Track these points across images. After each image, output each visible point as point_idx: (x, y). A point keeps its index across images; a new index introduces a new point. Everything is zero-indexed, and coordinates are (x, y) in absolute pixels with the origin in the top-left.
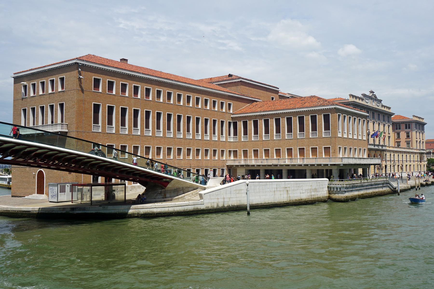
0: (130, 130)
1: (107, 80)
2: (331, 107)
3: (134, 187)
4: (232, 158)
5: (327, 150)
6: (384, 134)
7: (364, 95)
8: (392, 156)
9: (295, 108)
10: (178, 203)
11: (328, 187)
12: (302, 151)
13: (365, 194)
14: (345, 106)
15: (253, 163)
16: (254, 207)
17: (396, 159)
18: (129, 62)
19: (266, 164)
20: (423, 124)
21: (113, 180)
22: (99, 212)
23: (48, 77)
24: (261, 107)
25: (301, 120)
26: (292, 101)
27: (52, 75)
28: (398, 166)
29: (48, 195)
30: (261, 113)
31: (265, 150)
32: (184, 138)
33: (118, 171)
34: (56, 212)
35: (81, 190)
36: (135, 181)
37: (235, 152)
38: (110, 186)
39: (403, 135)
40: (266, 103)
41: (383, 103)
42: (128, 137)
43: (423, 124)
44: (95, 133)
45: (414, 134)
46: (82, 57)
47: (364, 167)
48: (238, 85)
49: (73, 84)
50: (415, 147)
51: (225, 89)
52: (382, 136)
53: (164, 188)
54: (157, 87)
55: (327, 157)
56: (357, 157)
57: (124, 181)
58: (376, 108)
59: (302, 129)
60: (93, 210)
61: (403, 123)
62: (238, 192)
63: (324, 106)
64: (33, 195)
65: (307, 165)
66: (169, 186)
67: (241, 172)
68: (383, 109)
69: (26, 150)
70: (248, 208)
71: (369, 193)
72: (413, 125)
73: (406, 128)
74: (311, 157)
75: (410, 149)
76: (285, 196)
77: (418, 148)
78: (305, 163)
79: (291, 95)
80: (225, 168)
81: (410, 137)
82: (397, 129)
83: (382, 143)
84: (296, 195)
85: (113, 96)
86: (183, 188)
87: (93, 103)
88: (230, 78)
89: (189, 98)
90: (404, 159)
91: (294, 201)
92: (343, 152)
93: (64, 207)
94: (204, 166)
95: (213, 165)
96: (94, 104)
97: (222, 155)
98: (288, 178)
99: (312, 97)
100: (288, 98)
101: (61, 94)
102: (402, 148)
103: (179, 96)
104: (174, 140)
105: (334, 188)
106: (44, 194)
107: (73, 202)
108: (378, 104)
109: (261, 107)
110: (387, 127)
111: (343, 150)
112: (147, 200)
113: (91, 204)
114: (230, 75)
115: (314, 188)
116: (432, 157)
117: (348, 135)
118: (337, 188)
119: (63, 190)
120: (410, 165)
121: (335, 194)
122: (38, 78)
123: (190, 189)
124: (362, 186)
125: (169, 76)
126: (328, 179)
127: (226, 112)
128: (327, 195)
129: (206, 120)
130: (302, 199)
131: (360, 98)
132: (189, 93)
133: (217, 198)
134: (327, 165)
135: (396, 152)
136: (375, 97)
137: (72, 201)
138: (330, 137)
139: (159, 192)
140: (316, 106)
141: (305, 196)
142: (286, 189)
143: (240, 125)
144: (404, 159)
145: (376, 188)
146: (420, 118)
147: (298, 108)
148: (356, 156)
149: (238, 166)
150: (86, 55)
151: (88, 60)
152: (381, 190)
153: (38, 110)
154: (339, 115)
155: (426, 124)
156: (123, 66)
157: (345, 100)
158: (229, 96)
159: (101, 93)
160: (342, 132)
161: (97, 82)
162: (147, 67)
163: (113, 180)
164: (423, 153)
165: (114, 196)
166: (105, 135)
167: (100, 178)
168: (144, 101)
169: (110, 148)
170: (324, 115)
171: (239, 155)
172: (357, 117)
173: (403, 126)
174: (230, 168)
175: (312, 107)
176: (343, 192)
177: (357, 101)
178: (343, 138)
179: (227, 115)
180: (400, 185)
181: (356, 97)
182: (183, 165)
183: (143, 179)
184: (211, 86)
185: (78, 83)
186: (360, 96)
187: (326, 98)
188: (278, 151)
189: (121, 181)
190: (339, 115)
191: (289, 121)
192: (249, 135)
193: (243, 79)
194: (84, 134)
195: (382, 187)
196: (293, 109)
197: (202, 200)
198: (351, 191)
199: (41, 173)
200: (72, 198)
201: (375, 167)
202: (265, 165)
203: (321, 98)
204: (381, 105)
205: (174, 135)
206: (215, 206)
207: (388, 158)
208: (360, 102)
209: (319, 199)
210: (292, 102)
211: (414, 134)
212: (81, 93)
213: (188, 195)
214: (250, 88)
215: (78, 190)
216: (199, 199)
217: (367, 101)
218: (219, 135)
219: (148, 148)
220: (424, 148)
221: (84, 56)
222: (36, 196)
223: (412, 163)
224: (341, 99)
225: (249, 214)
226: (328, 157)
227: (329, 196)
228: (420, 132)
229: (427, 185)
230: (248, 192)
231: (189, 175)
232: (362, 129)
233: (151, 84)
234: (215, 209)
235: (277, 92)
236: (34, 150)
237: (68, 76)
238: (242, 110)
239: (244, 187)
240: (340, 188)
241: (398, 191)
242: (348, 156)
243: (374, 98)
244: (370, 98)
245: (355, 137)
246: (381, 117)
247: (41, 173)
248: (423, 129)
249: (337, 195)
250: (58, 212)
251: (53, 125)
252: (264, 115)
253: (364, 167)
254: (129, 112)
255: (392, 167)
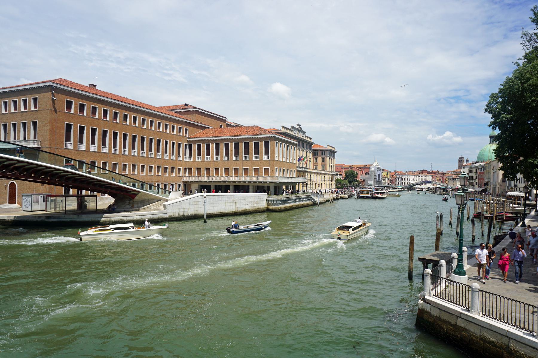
0: (110, 150)
1: (79, 102)
2: (271, 136)
3: (103, 198)
4: (187, 175)
5: (266, 170)
6: (307, 159)
7: (293, 127)
8: (312, 177)
9: (242, 136)
10: (145, 213)
11: (267, 200)
12: (246, 170)
13: (294, 206)
14: (279, 135)
15: (205, 179)
16: (211, 216)
17: (315, 179)
18: (97, 88)
19: (216, 180)
20: (334, 152)
21: (84, 192)
22: (73, 220)
23: (21, 97)
24: (212, 133)
25: (246, 145)
26: (238, 129)
27: (25, 95)
28: (316, 184)
29: (21, 205)
30: (213, 138)
31: (216, 169)
32: (147, 157)
33: (92, 184)
34: (32, 220)
35: (55, 200)
36: (104, 193)
37: (190, 170)
38: (82, 198)
39: (320, 160)
40: (217, 130)
41: (307, 134)
42: (98, 155)
43: (334, 152)
44: (67, 150)
45: (328, 160)
46: (55, 80)
47: (287, 185)
48: (193, 114)
49: (47, 105)
50: (328, 170)
51: (180, 116)
52: (305, 161)
53: (132, 199)
54: (124, 111)
55: (266, 176)
56: (288, 176)
57: (94, 193)
58: (301, 138)
59: (246, 153)
60: (68, 219)
61: (320, 150)
62: (195, 203)
63: (265, 134)
64: (5, 204)
65: (251, 182)
66: (137, 198)
67: (195, 187)
68: (306, 139)
69: (5, 163)
70: (205, 217)
71: (297, 205)
72: (327, 153)
73: (322, 155)
74: (253, 175)
75: (324, 171)
76: (234, 207)
77: (331, 170)
78: (249, 180)
79: (236, 124)
80: (181, 183)
81: (325, 162)
82: (315, 155)
83: (305, 166)
84: (242, 206)
85: (84, 118)
86: (148, 199)
87: (65, 122)
88: (186, 107)
89: (159, 124)
90: (320, 179)
91: (241, 211)
92: (278, 172)
93: (40, 216)
94: (164, 181)
95: (171, 181)
96: (66, 123)
97: (179, 172)
98: (235, 192)
99: (255, 127)
100: (234, 126)
101: (33, 112)
102: (319, 170)
103: (143, 120)
104: (138, 158)
105: (271, 201)
106: (15, 204)
107: (47, 211)
108: (303, 135)
109: (212, 133)
110: (309, 153)
111: (278, 170)
112: (118, 210)
113: (65, 213)
114: (186, 105)
115: (256, 200)
116: (338, 178)
117: (283, 159)
118: (274, 201)
119: (36, 200)
120: (324, 184)
121: (272, 205)
122: (10, 97)
123: (154, 201)
124: (293, 199)
125: (134, 103)
126: (267, 194)
127: (183, 136)
128: (266, 206)
129: (166, 142)
130: (247, 210)
131: (290, 130)
132: (152, 118)
133: (178, 208)
134: (267, 182)
135: (315, 173)
136: (301, 129)
137: (46, 210)
138: (269, 160)
139: (128, 203)
140: (258, 135)
141: (248, 207)
142: (234, 202)
143: (195, 148)
144: (320, 179)
145: (302, 201)
146: (332, 147)
147: (244, 135)
148: (288, 176)
149: (192, 182)
150: (58, 79)
151: (61, 83)
152: (305, 202)
153: (9, 126)
154: (277, 143)
155: (336, 152)
156: (92, 90)
157: (278, 130)
158: (186, 122)
159: (73, 114)
160: (279, 157)
161: (69, 104)
162: (114, 94)
163: (84, 192)
164: (333, 175)
165: (86, 206)
166: (76, 152)
167: (71, 190)
168: (112, 123)
169: (81, 163)
170: (265, 142)
171: (193, 173)
172: (290, 145)
173: (320, 153)
174: (186, 184)
175: (255, 135)
176: (279, 204)
177: (288, 131)
178: (278, 161)
179: (184, 139)
180: (319, 199)
181: (287, 129)
182: (145, 180)
183: (114, 192)
184: (168, 112)
185: (51, 103)
186: (290, 128)
187: (265, 128)
188: (227, 170)
189: (90, 193)
190: (277, 143)
191: (236, 145)
192: (202, 155)
193: (197, 108)
194: (57, 151)
195: (306, 200)
196: (240, 136)
197: (166, 210)
198: (285, 203)
199: (12, 185)
200: (46, 208)
201: (299, 185)
202: (216, 182)
203: (262, 128)
204: (305, 135)
205: (139, 153)
206: (177, 215)
207: (309, 178)
208: (290, 132)
209: (260, 209)
210: (238, 130)
211: (328, 160)
212: (54, 113)
213: (152, 206)
214: (203, 117)
215: (52, 201)
216: (163, 209)
217: (295, 132)
218: (176, 155)
219: (115, 165)
220: (335, 171)
221: (56, 80)
222: (7, 205)
223: (326, 182)
224: (275, 130)
225: (205, 222)
226: (267, 176)
227: (267, 207)
228: (330, 158)
229: (337, 199)
230: (205, 203)
231: (150, 188)
232: (293, 154)
233: (119, 108)
234: (177, 218)
235: (225, 121)
236: (13, 163)
237: (42, 97)
238: (197, 135)
239: (201, 200)
240: (276, 201)
241: (318, 203)
242: (282, 175)
243: (300, 130)
244: (297, 130)
245: (288, 161)
246: (305, 145)
247: (12, 185)
248: (334, 156)
249: (273, 206)
250: (34, 220)
251: (26, 141)
252: (215, 140)
253: (287, 185)
254: (98, 132)
255: (311, 185)
